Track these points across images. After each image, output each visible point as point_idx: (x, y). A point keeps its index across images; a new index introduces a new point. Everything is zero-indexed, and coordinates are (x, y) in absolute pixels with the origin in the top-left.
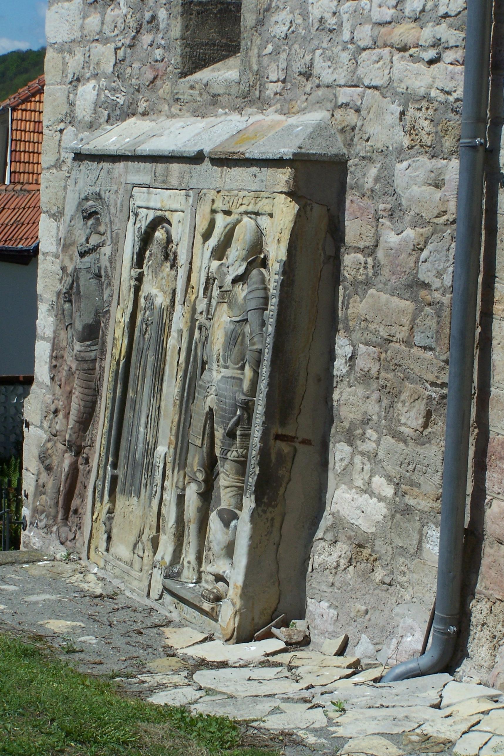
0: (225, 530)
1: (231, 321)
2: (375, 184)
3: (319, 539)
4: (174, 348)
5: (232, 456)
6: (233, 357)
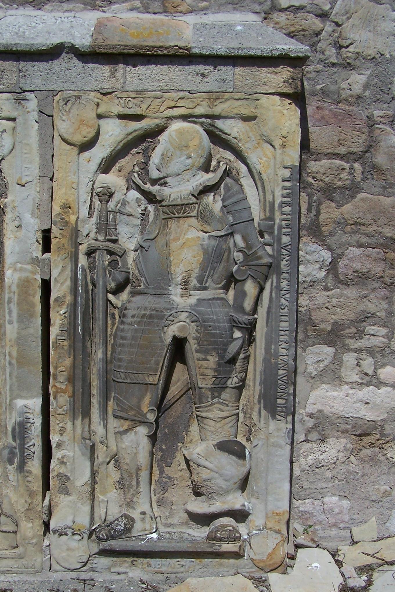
0: (241, 462)
1: (210, 237)
2: (364, 91)
3: (301, 442)
4: (24, 285)
5: (233, 383)
6: (216, 276)
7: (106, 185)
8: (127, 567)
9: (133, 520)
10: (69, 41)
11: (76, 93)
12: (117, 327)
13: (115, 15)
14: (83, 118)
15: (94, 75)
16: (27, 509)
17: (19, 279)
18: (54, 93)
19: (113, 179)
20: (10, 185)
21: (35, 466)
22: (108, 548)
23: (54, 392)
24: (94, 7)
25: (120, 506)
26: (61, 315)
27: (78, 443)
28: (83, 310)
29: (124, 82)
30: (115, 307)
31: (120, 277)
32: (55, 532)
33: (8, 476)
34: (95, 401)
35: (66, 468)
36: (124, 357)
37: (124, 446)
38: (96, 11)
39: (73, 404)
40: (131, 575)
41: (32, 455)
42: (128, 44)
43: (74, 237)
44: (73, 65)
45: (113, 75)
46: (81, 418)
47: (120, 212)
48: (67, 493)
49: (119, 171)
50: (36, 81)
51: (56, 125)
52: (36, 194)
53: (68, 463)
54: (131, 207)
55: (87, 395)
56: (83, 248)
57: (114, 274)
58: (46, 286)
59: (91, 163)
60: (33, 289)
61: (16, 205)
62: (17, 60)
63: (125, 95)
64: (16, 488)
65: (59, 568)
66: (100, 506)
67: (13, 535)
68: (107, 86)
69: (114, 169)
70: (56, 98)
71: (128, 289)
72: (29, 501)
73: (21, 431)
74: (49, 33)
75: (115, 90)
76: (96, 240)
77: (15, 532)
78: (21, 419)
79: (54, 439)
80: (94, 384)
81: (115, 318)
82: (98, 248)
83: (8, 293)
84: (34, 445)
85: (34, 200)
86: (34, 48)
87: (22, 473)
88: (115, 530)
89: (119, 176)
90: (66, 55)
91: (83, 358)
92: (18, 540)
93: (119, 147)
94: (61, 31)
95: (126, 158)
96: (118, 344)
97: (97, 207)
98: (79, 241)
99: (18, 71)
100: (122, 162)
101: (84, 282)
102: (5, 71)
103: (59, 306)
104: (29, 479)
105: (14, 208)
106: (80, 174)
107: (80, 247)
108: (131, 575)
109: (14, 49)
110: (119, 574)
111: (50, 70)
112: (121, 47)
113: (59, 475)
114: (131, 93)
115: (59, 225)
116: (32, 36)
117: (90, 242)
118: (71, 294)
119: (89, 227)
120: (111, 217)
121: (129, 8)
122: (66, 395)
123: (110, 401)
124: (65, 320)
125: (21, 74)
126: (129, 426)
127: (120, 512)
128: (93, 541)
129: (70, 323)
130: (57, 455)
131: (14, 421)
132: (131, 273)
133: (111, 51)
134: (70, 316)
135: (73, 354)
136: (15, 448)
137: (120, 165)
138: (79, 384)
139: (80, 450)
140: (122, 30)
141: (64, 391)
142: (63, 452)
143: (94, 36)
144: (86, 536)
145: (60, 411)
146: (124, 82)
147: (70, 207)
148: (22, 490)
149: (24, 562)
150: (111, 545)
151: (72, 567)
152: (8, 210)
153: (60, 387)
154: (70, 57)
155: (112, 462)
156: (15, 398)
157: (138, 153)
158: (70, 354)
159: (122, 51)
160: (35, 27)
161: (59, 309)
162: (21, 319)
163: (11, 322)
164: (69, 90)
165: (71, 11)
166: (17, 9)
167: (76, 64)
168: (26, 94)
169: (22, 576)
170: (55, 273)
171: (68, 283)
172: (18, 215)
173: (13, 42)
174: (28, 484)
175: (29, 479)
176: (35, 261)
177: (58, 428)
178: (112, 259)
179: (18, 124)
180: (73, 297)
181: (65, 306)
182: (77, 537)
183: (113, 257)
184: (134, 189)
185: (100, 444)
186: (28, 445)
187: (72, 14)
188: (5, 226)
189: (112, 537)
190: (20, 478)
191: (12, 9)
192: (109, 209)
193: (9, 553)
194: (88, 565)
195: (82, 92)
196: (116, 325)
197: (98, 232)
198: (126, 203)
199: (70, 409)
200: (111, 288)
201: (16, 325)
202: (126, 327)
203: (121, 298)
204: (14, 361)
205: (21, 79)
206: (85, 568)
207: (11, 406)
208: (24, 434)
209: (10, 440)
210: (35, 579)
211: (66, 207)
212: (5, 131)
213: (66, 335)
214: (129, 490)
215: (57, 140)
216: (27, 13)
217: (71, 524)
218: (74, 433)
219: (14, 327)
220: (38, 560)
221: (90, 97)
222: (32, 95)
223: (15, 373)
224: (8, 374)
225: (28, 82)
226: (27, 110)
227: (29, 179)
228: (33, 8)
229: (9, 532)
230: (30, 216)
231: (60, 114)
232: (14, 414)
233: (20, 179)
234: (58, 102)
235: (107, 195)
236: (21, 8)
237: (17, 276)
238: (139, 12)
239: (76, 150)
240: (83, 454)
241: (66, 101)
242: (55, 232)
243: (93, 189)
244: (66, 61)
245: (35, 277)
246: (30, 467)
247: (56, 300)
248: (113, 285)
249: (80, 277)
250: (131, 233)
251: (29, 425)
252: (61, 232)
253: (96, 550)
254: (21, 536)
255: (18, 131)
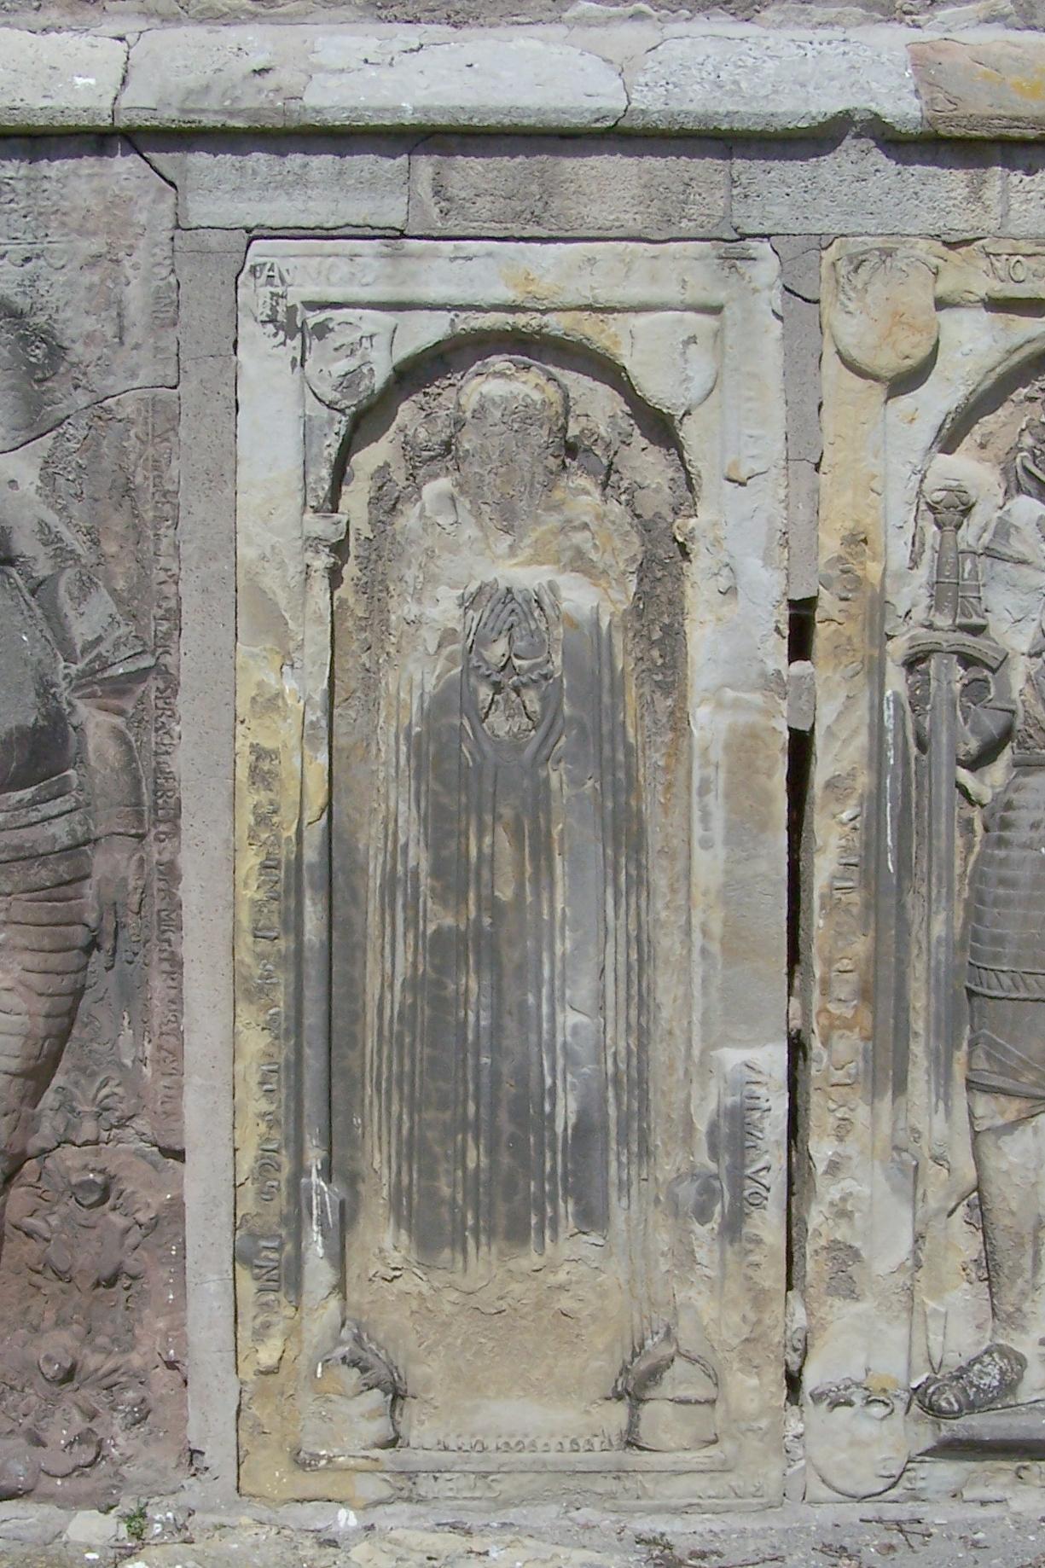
4: (744, 745)
7: (955, 483)
8: (1005, 1486)
9: (1021, 1361)
10: (866, 106)
11: (878, 242)
12: (981, 855)
13: (947, 35)
14: (902, 309)
15: (926, 194)
16: (747, 1340)
17: (732, 729)
18: (823, 242)
19: (968, 468)
20: (704, 481)
21: (768, 1225)
22: (963, 1434)
23: (822, 1028)
24: (891, 14)
25: (978, 1327)
26: (843, 824)
27: (882, 1161)
28: (897, 811)
29: (1005, 215)
30: (972, 803)
31: (992, 724)
32: (817, 1398)
33: (693, 1252)
34: (918, 1049)
35: (852, 1226)
36: (1010, 932)
37: (1004, 1166)
38: (896, 25)
39: (871, 1058)
40: (1016, 1505)
41: (765, 1194)
42: (1021, 114)
43: (877, 618)
44: (872, 169)
45: (975, 195)
46: (890, 1093)
47: (989, 552)
48: (852, 1295)
49: (983, 446)
50: (775, 209)
51: (830, 327)
52: (777, 505)
53: (857, 1215)
54: (1025, 542)
55: (902, 1032)
56: (898, 649)
57: (977, 714)
58: (800, 747)
59: (916, 424)
60: (768, 757)
61: (721, 534)
62: (727, 155)
63: (1005, 247)
64: (716, 1287)
65: (823, 1492)
66: (927, 1329)
67: (704, 1410)
68: (960, 223)
69: (968, 442)
70: (829, 255)
71: (1006, 755)
72: (752, 1316)
73: (735, 1131)
74: (803, 85)
75: (979, 234)
76: (930, 626)
77: (711, 1402)
78: (737, 1098)
79: (821, 1149)
80: (918, 1005)
81: (973, 831)
82: (937, 647)
83: (701, 767)
84: (768, 1169)
85: (770, 520)
86: (778, 124)
87: (736, 1246)
88: (978, 1387)
89: (982, 460)
90: (854, 142)
91: (897, 935)
92: (719, 1423)
93: (988, 383)
94: (832, 79)
95: (999, 412)
96: (989, 899)
97: (929, 541)
98: (887, 629)
99: (728, 182)
100: (988, 423)
101: (900, 738)
102: (693, 183)
103: (837, 800)
104: (754, 1258)
105: (717, 541)
106: (890, 458)
107: (890, 646)
108: (1016, 1505)
109: (724, 127)
110: (983, 1503)
111: (813, 180)
112: (1004, 122)
113: (834, 1246)
114: (1022, 242)
115: (838, 588)
116: (763, 92)
117: (912, 633)
118: (870, 767)
119: (911, 594)
120: (968, 566)
121: (981, 16)
122: (855, 1036)
123: (959, 1047)
124: (855, 836)
125: (735, 192)
126: (1019, 1111)
127: (979, 1343)
128: (917, 1420)
129: (867, 846)
130: (828, 1191)
131: (712, 1105)
132: (1021, 713)
133: (978, 133)
134: (867, 827)
135: (873, 926)
136: (717, 1177)
137: (985, 430)
138: (887, 1004)
139: (888, 1178)
140: (986, 76)
141: (848, 1025)
142: (844, 1184)
143: (922, 91)
144: (900, 1406)
145: (838, 1076)
146: (1005, 215)
147: (865, 541)
148: (733, 1288)
149: (732, 1479)
150: (971, 1427)
151: (863, 1491)
152: (697, 548)
153: (838, 1012)
154: (864, 147)
155: (962, 1210)
156: (715, 1047)
157: (1032, 399)
158: (866, 926)
159: (1004, 131)
160: (755, 69)
161: (835, 808)
162: (734, 834)
163: (707, 844)
164: (861, 235)
165: (831, 24)
166: (687, 19)
167: (880, 167)
168: (748, 242)
169: (729, 1518)
170: (827, 714)
171: (863, 739)
172: (727, 560)
173: (722, 110)
174: (750, 1272)
175: (754, 1258)
176: (775, 684)
177: (831, 1121)
178: (971, 676)
179: (729, 323)
180: (875, 775)
181: (853, 801)
182: (878, 1410)
183: (975, 673)
184: (1029, 494)
185: (931, 1162)
186: (753, 1169)
187: (837, 33)
188: (689, 591)
189: (972, 1407)
190: (729, 1255)
191: (675, 21)
192: (963, 546)
193: (697, 1457)
194: (904, 1483)
195: (894, 238)
196: (977, 849)
197: (937, 604)
198: (1012, 530)
199: (866, 1071)
200: (968, 753)
201: (721, 851)
202: (1015, 854)
203: (988, 780)
204: (715, 948)
205: (735, 206)
206: (893, 1493)
207: (707, 1067)
208: (744, 1140)
209: (703, 1158)
210: (766, 1525)
211: (858, 540)
212: (693, 340)
213: (856, 876)
214: (1013, 1282)
215: (832, 364)
216: (718, 30)
217: (859, 1375)
218: (873, 1134)
219: (715, 857)
220: (772, 1473)
221: (917, 252)
222: (764, 248)
223: (717, 981)
224: (697, 980)
225: (755, 213)
226: (752, 285)
227: (758, 468)
228: (732, 18)
229: (698, 1402)
230: (760, 563)
231: (842, 297)
232: (714, 1087)
233: (735, 465)
234: (834, 264)
235: (954, 509)
236: (700, 17)
237: (724, 721)
238: (1007, 27)
239: (880, 391)
240: (896, 1190)
241: (856, 262)
242: (828, 604)
243: (920, 493)
244: (854, 157)
245: (773, 723)
246: (756, 1226)
247: (830, 785)
248: (974, 745)
249: (889, 723)
250: (1022, 609)
251: (757, 1114)
252: (844, 604)
253: (928, 1442)
254: (727, 1412)
255: (728, 341)
